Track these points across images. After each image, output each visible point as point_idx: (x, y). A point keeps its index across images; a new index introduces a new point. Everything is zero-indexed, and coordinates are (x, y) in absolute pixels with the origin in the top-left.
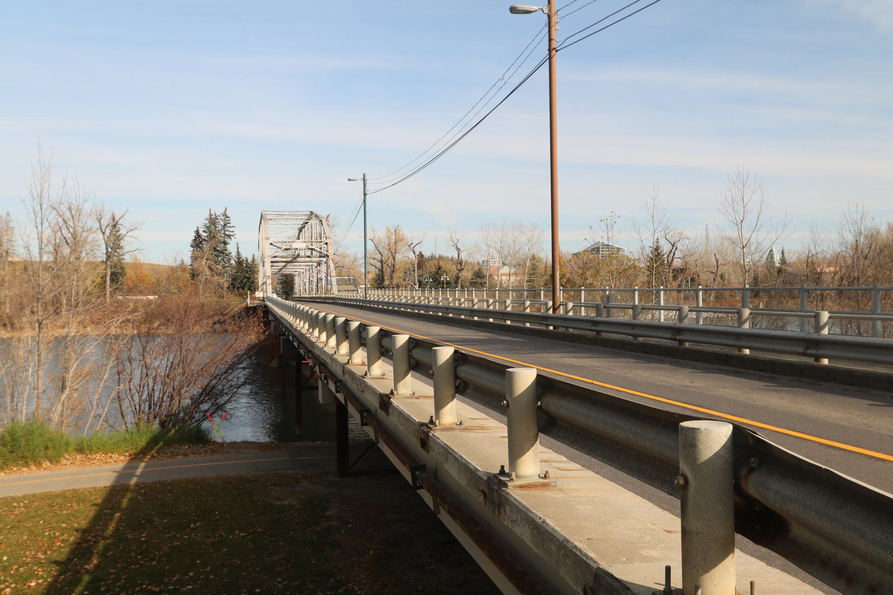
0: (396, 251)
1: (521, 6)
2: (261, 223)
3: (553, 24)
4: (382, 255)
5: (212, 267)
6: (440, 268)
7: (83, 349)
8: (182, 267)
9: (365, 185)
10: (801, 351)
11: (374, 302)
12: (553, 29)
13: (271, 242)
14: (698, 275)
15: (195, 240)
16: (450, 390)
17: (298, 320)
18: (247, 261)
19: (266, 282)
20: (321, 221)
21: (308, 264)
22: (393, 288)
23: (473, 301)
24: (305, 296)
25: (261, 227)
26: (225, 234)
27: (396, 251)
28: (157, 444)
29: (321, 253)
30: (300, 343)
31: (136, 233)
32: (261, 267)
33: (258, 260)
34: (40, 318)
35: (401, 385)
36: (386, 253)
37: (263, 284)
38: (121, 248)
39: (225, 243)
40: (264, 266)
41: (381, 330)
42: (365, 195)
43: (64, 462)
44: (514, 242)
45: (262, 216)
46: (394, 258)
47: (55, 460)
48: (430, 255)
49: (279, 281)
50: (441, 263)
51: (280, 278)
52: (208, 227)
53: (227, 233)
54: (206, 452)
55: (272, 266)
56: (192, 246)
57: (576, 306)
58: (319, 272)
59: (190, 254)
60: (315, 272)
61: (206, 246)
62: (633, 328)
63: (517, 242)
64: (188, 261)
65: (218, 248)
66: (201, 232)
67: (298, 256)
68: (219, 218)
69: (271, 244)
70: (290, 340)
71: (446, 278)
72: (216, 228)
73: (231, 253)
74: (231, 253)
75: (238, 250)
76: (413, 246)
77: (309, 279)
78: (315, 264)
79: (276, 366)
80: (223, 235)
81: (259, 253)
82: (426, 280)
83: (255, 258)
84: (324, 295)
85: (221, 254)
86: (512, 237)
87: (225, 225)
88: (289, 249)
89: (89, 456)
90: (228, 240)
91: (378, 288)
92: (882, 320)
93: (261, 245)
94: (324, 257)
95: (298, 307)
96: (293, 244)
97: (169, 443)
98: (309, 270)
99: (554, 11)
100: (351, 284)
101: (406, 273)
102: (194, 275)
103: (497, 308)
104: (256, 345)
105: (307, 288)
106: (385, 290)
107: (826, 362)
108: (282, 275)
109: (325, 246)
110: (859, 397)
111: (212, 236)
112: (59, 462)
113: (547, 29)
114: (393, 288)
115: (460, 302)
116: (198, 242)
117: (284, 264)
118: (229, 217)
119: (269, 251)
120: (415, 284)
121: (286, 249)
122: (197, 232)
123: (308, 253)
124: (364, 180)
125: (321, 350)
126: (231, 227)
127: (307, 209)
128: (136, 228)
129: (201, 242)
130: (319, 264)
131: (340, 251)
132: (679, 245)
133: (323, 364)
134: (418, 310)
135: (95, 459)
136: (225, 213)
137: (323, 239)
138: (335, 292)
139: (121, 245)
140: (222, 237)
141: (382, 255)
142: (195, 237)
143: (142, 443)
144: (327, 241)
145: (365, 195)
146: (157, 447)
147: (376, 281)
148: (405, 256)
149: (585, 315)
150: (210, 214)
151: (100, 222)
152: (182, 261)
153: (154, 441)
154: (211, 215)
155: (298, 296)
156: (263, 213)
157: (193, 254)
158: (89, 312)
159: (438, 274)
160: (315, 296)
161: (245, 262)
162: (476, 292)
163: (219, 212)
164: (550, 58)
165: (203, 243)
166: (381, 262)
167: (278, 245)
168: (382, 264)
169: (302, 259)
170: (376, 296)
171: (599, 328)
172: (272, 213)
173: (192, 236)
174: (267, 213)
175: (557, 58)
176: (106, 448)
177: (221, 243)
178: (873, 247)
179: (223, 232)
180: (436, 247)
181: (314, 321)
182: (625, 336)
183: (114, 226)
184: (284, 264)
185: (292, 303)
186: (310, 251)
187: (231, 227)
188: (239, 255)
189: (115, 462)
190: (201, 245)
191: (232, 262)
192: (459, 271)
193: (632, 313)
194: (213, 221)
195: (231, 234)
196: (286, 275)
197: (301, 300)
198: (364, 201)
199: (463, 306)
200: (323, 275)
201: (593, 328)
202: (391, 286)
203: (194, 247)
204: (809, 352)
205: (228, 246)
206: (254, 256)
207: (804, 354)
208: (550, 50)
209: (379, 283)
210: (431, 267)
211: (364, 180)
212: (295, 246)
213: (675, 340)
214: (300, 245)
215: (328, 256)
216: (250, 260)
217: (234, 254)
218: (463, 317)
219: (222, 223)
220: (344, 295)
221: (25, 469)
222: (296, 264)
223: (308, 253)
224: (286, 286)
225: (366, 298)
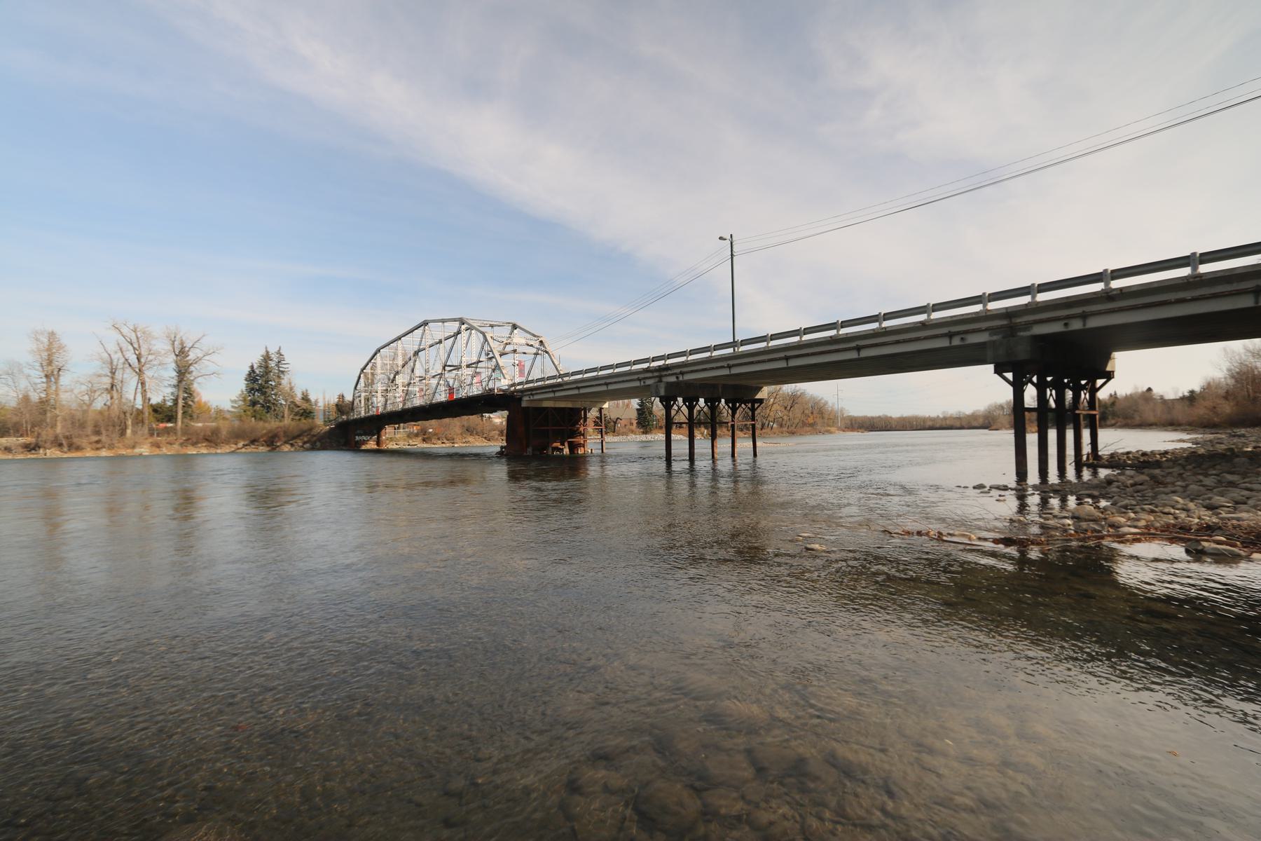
2: (411, 331)
7: (46, 423)
15: (249, 374)
31: (214, 357)
53: (281, 369)
56: (246, 380)
66: (255, 367)
87: (279, 362)
122: (252, 367)
128: (214, 352)
136: (279, 351)
158: (606, 722)
173: (247, 370)
193: (1071, 396)
194: (267, 358)
195: (286, 370)
216: (261, 358)
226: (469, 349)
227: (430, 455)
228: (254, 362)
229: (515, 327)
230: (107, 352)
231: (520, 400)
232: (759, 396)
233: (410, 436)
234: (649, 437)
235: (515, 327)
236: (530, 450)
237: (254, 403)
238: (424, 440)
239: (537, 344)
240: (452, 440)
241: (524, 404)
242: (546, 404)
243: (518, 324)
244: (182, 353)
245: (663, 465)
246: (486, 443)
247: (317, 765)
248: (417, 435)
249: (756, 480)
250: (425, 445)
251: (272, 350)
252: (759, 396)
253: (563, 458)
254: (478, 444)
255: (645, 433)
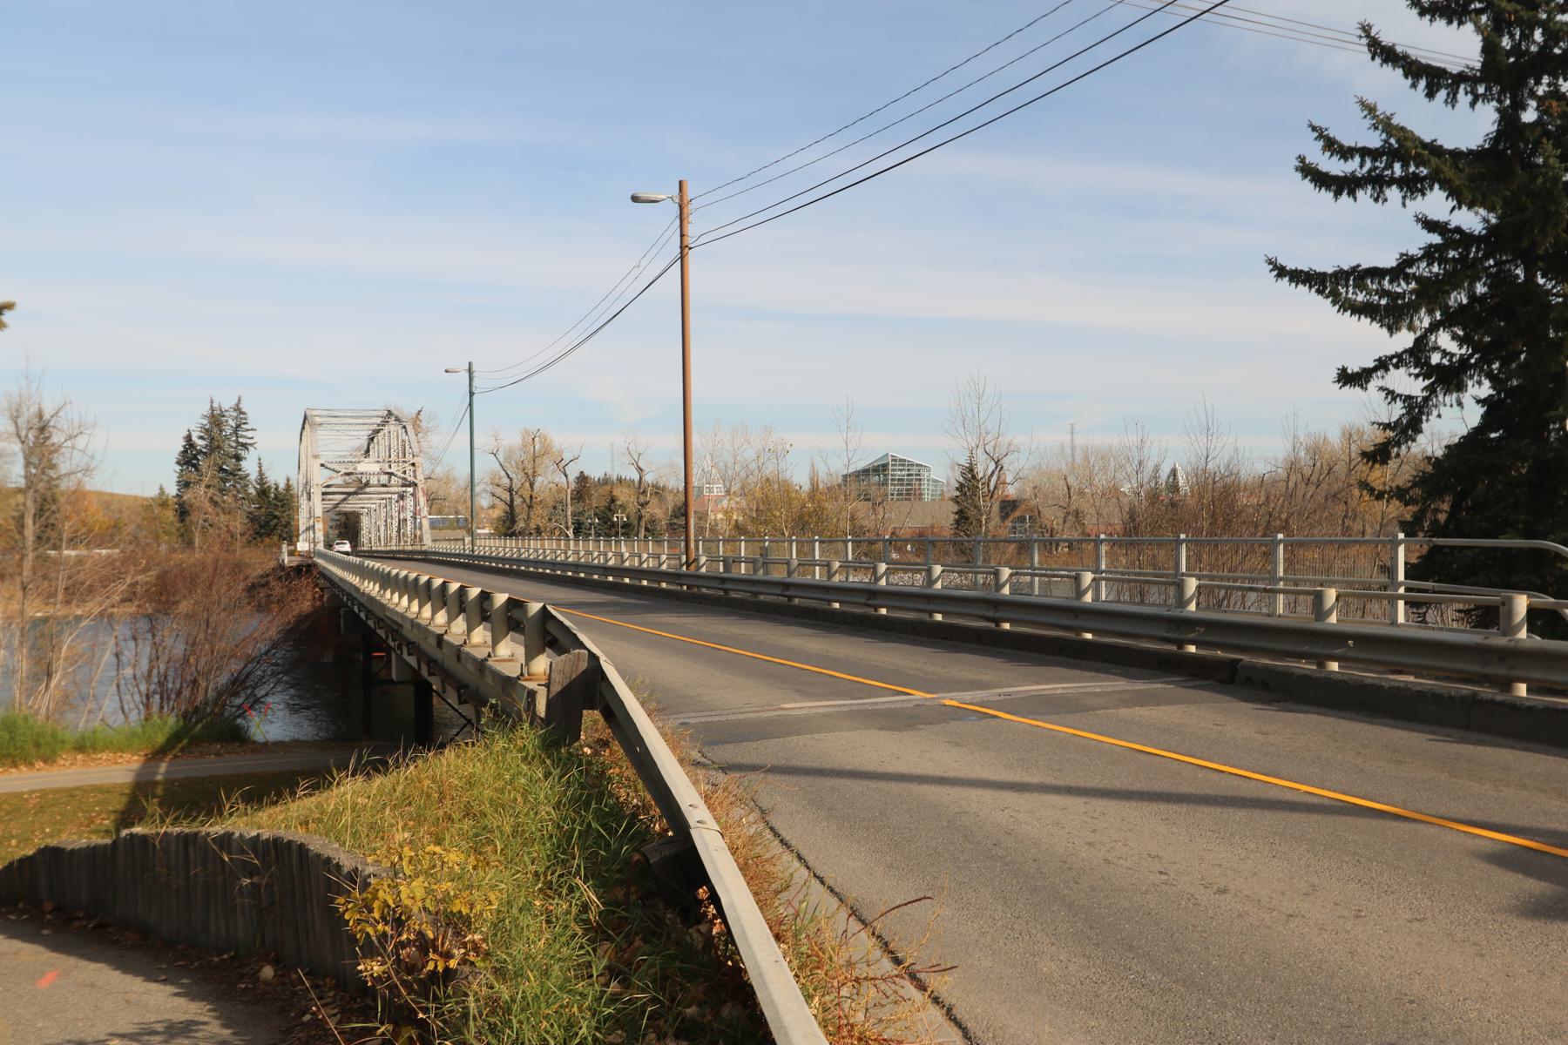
0: (534, 472)
1: (643, 194)
2: (303, 428)
3: (685, 216)
4: (511, 480)
5: (215, 498)
6: (613, 501)
8: (163, 502)
9: (471, 379)
10: (863, 601)
11: (484, 558)
12: (685, 222)
13: (323, 462)
14: (1039, 512)
15: (185, 452)
16: (478, 619)
17: (366, 582)
18: (276, 489)
19: (314, 526)
20: (404, 427)
21: (384, 496)
22: (531, 534)
23: (622, 556)
24: (379, 549)
25: (304, 434)
26: (237, 442)
27: (534, 472)
28: (180, 742)
29: (404, 479)
30: (369, 612)
32: (303, 501)
33: (298, 488)
34: (25, 580)
35: (453, 624)
36: (518, 480)
37: (308, 529)
38: (53, 467)
39: (238, 458)
40: (309, 499)
41: (482, 592)
42: (471, 394)
43: (62, 762)
44: (735, 457)
45: (305, 418)
46: (532, 485)
47: (49, 759)
48: (602, 476)
49: (334, 524)
50: (616, 492)
51: (337, 518)
52: (207, 430)
53: (241, 440)
54: (245, 752)
55: (323, 500)
56: (178, 463)
57: (948, 571)
58: (402, 509)
59: (174, 478)
60: (395, 507)
61: (203, 463)
62: (1076, 616)
63: (738, 458)
64: (172, 490)
65: (224, 467)
66: (194, 438)
67: (367, 484)
68: (227, 414)
69: (322, 465)
70: (353, 611)
71: (622, 518)
72: (221, 431)
73: (248, 475)
74: (248, 475)
75: (261, 471)
76: (563, 463)
77: (386, 521)
78: (395, 497)
79: (331, 661)
80: (234, 444)
81: (301, 477)
82: (589, 521)
83: (291, 482)
84: (410, 548)
85: (231, 477)
86: (731, 449)
87: (238, 426)
88: (352, 473)
89: (93, 756)
90: (243, 453)
91: (506, 535)
92: (1041, 575)
93: (303, 465)
94: (410, 486)
95: (366, 564)
96: (359, 465)
97: (196, 741)
98: (386, 506)
99: (685, 201)
100: (460, 528)
101: (555, 508)
102: (183, 511)
103: (817, 577)
104: (307, 616)
105: (382, 536)
106: (523, 540)
107: (1007, 626)
108: (339, 513)
109: (411, 467)
110: (856, 636)
111: (214, 446)
112: (54, 761)
113: (678, 221)
114: (531, 534)
115: (829, 571)
116: (190, 455)
117: (343, 496)
118: (244, 413)
119: (319, 477)
120: (567, 528)
121: (348, 474)
122: (189, 438)
123: (384, 479)
124: (470, 371)
125: (393, 611)
126: (248, 430)
127: (380, 404)
129: (195, 457)
130: (402, 497)
131: (440, 471)
132: (1005, 462)
133: (395, 626)
134: (562, 571)
135: (101, 759)
136: (237, 405)
137: (409, 457)
138: (428, 544)
139: (54, 462)
140: (232, 447)
141: (511, 480)
142: (184, 447)
143: (161, 739)
144: (415, 460)
145: (471, 394)
146: (180, 746)
147: (504, 522)
148: (549, 481)
149: (1111, 598)
150: (212, 407)
151: (16, 423)
152: (161, 489)
153: (174, 739)
154: (212, 409)
155: (366, 549)
156: (308, 414)
157: (181, 476)
159: (610, 510)
160: (394, 548)
161: (273, 490)
162: (749, 544)
163: (227, 403)
164: (682, 257)
165: (199, 457)
166: (510, 490)
167: (332, 466)
168: (511, 495)
169: (372, 489)
170: (487, 549)
171: (728, 586)
172: (323, 413)
173: (179, 445)
174: (315, 413)
175: (692, 256)
176: (117, 747)
177: (231, 458)
178: (1318, 464)
179: (234, 438)
180: (612, 461)
181: (387, 581)
182: (776, 597)
183: (42, 429)
184: (343, 496)
185: (358, 559)
186: (387, 476)
187: (248, 430)
188: (262, 479)
189: (128, 762)
190: (195, 462)
191: (252, 490)
192: (642, 505)
194: (216, 419)
196: (346, 514)
197: (372, 555)
198: (471, 405)
199: (645, 565)
200: (409, 515)
201: (721, 586)
202: (527, 532)
203: (182, 465)
204: (869, 602)
205: (243, 464)
206: (288, 480)
207: (866, 605)
208: (682, 248)
209: (508, 526)
210: (597, 500)
211: (470, 371)
212: (361, 468)
213: (784, 596)
214: (368, 467)
215: (416, 485)
216: (282, 486)
217: (253, 476)
218: (596, 577)
219: (233, 423)
220: (443, 547)
221: (13, 770)
222: (364, 496)
223: (384, 479)
224: (347, 527)
225: (473, 551)
227: (1265, 686)
230: (462, 716)
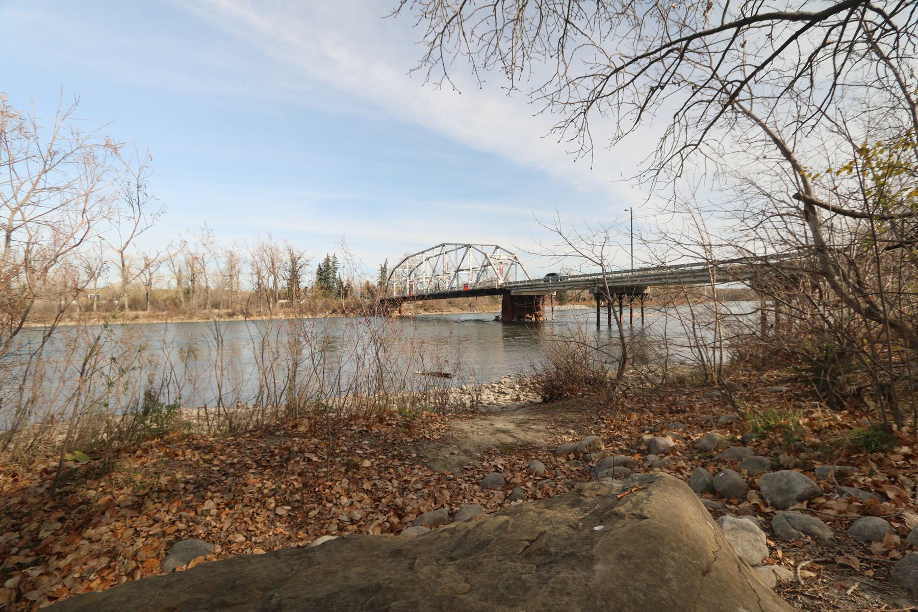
194: (328, 260)
226: (474, 260)
228: (238, 253)
229: (497, 247)
231: (510, 291)
232: (645, 292)
233: (417, 307)
234: (564, 307)
235: (497, 247)
236: (515, 318)
237: (322, 288)
238: (425, 310)
239: (512, 258)
240: (441, 310)
241: (512, 294)
242: (523, 294)
243: (500, 246)
244: (294, 262)
245: (74, 244)
246: (461, 312)
247: (817, 539)
248: (421, 307)
249: (642, 332)
250: (426, 313)
251: (331, 255)
252: (645, 292)
253: (532, 323)
254: (456, 312)
255: (561, 304)
